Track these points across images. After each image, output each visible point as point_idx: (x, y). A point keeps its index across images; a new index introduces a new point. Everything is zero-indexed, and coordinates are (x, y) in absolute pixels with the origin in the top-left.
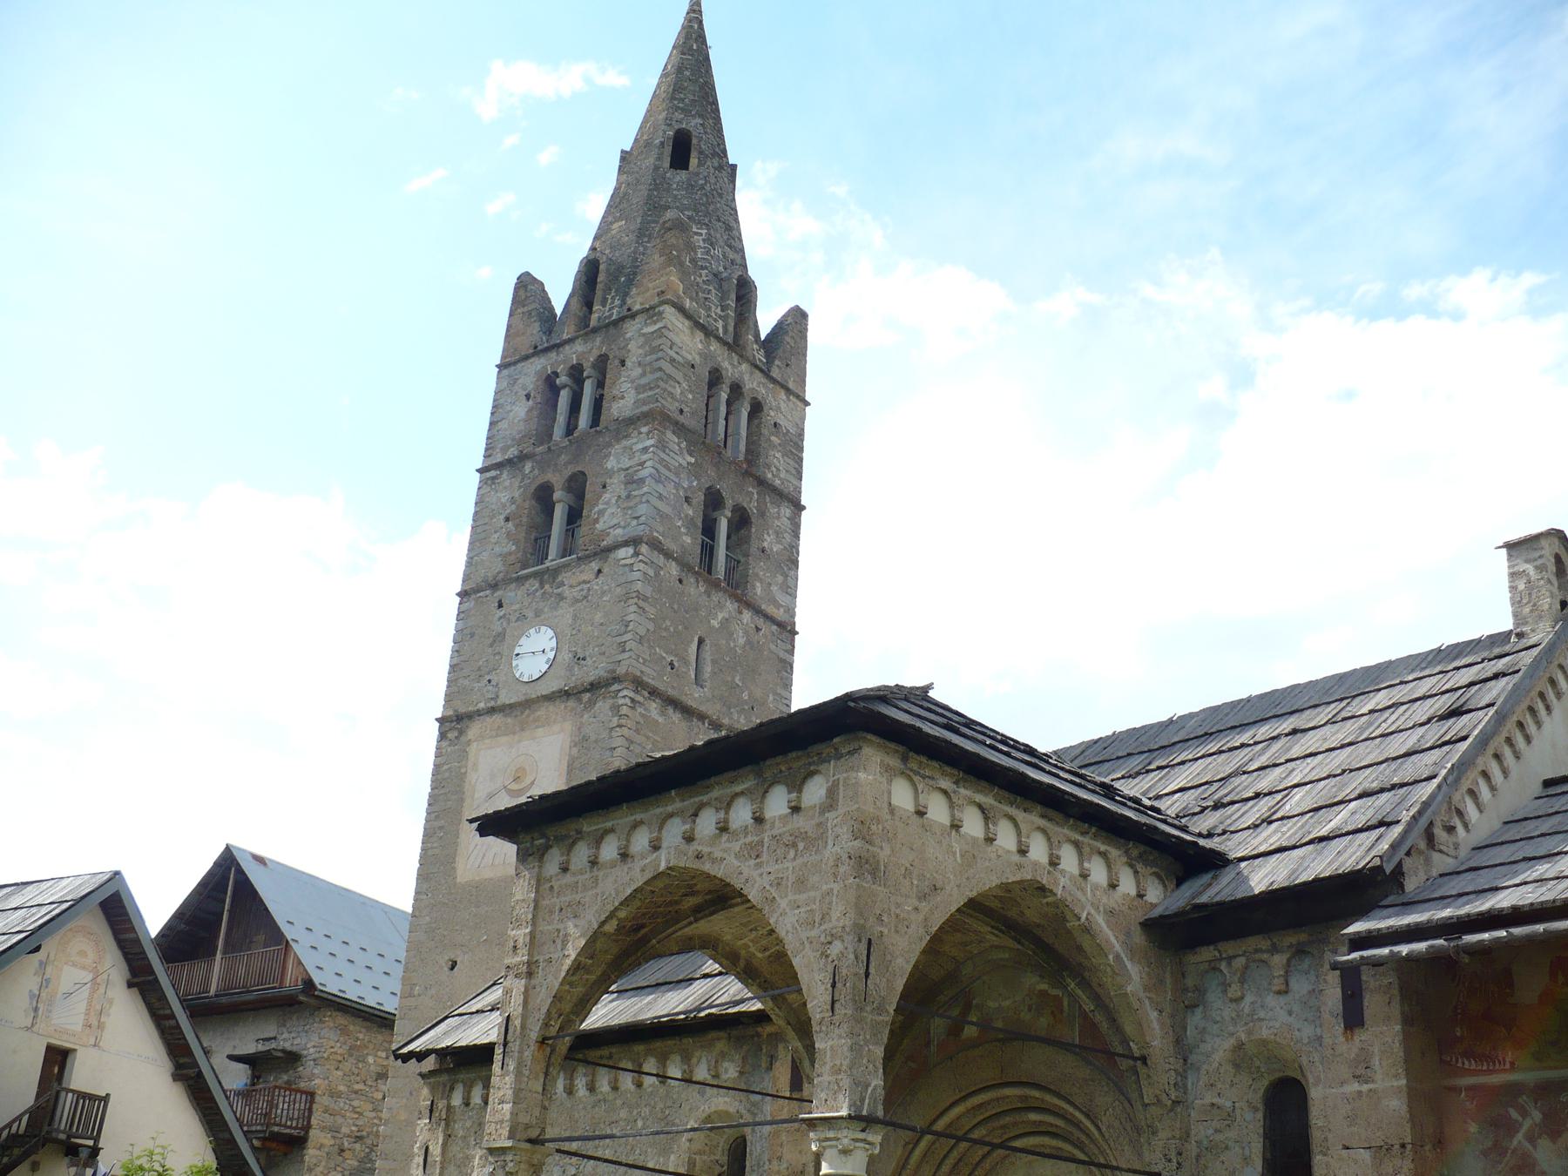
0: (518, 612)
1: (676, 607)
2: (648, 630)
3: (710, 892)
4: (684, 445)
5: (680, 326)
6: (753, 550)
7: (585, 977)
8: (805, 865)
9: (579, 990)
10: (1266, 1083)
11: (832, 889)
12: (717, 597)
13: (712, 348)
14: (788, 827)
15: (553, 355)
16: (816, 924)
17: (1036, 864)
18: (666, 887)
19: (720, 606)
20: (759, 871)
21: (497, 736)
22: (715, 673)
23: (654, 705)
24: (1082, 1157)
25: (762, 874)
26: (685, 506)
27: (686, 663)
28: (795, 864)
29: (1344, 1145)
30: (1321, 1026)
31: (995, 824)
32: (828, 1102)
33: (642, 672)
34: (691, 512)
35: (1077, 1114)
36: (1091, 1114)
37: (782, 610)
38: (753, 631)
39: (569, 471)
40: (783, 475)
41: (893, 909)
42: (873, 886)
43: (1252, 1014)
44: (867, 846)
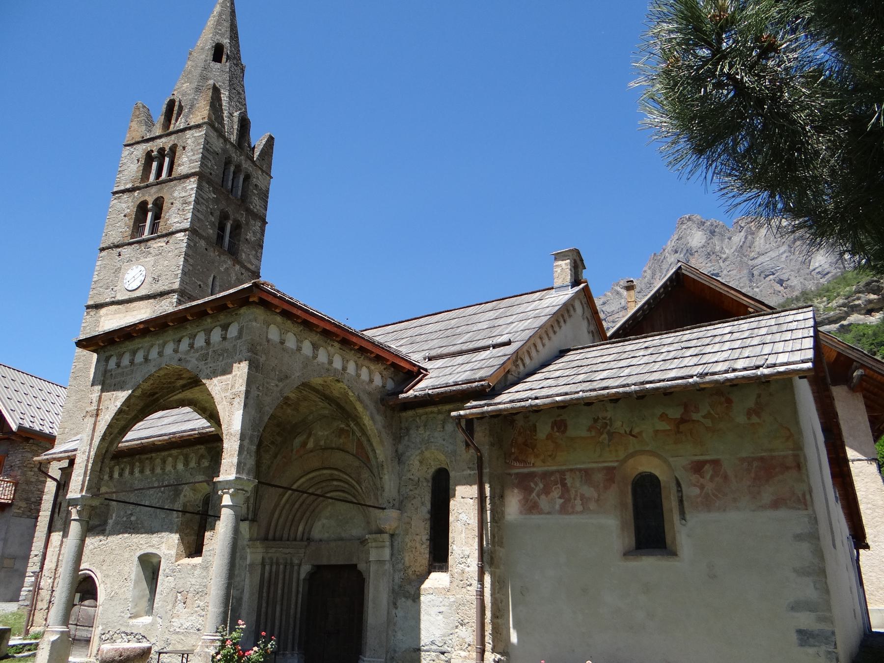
1: (203, 260)
3: (190, 378)
4: (211, 189)
6: (242, 239)
7: (125, 416)
9: (122, 423)
12: (223, 258)
14: (221, 346)
15: (151, 143)
17: (335, 369)
18: (165, 375)
19: (225, 262)
20: (207, 366)
24: (356, 501)
25: (207, 368)
27: (207, 285)
31: (318, 350)
34: (213, 220)
35: (353, 482)
37: (254, 266)
38: (239, 274)
39: (155, 197)
41: (265, 384)
42: (257, 374)
43: (429, 439)
44: (254, 356)
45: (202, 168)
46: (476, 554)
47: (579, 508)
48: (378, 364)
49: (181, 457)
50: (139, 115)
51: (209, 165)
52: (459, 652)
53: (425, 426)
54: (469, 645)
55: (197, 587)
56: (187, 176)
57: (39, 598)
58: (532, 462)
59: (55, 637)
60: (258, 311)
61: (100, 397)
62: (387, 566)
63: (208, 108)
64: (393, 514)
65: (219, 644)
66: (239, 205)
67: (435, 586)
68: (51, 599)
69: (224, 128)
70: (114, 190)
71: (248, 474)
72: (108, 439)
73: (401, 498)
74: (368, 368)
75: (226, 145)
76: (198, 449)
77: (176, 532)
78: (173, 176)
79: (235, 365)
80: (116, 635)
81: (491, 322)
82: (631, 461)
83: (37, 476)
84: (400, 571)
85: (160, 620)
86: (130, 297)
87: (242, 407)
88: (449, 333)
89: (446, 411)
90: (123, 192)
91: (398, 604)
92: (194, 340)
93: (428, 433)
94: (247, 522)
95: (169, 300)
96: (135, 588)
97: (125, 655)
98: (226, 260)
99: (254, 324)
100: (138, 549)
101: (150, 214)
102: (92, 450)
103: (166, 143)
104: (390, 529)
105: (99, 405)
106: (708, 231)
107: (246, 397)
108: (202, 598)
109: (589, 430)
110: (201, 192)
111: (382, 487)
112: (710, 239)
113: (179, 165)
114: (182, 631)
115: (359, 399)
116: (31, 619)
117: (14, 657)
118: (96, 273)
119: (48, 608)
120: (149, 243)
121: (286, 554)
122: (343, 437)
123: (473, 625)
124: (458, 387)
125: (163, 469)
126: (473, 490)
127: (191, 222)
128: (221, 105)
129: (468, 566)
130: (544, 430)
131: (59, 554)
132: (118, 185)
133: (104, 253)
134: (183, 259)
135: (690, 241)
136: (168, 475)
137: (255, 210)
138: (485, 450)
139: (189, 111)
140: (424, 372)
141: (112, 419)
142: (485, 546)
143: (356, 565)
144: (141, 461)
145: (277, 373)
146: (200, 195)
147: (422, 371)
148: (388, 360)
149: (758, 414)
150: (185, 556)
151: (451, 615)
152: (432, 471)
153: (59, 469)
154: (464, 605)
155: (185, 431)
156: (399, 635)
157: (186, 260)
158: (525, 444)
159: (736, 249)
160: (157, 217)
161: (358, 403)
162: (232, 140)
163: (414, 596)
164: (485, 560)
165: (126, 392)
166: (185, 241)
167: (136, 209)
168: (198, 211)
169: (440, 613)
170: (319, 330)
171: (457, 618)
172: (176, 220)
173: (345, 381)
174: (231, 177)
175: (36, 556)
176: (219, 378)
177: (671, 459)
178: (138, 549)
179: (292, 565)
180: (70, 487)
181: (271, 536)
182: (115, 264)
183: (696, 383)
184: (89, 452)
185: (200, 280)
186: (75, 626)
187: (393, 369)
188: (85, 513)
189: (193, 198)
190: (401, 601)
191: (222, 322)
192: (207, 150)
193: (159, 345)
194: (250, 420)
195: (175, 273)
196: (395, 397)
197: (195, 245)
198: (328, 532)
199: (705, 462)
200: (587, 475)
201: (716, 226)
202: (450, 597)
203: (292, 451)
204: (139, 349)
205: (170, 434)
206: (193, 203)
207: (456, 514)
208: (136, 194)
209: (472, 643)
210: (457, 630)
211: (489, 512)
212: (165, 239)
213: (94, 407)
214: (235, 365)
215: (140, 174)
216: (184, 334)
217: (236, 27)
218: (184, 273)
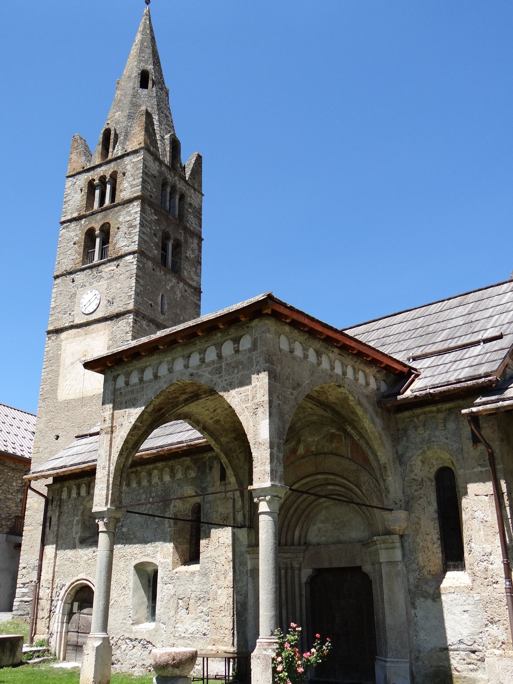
0: (82, 284)
1: (152, 280)
2: (141, 290)
3: (192, 392)
4: (153, 211)
5: (149, 159)
6: (183, 256)
8: (243, 375)
10: (436, 469)
11: (257, 385)
12: (168, 277)
13: (163, 169)
14: (234, 359)
15: (92, 172)
16: (250, 401)
17: (337, 375)
19: (171, 281)
20: (221, 379)
21: (75, 337)
22: (169, 309)
23: (145, 322)
25: (222, 381)
26: (154, 237)
27: (157, 304)
28: (238, 375)
29: (475, 494)
30: (462, 443)
31: (321, 357)
32: (261, 479)
33: (139, 308)
34: (157, 240)
35: (351, 485)
36: (358, 485)
39: (101, 223)
40: (194, 225)
42: (275, 383)
43: (430, 439)
44: (271, 366)
45: (143, 192)
46: (499, 551)
48: (372, 367)
49: (167, 469)
50: (77, 147)
51: (149, 188)
53: (424, 425)
54: (503, 643)
55: (198, 593)
56: (130, 201)
57: (39, 607)
59: (98, 643)
60: (269, 322)
61: (113, 415)
62: (400, 567)
63: (143, 133)
64: (402, 514)
65: (277, 646)
66: (177, 225)
67: (457, 585)
68: (51, 608)
69: (159, 152)
70: (62, 220)
71: (280, 481)
72: (125, 454)
73: (407, 499)
74: (364, 371)
75: (161, 167)
76: (184, 461)
77: (170, 541)
78: (116, 202)
79: (254, 377)
80: (120, 641)
81: (466, 317)
83: (5, 494)
84: (415, 571)
85: (162, 625)
86: (88, 320)
87: (268, 416)
88: (419, 332)
89: (446, 409)
90: (70, 221)
91: (416, 604)
92: (204, 354)
93: (428, 433)
94: (245, 529)
95: (125, 320)
96: (134, 596)
97: (178, 658)
98: (171, 278)
99: (268, 335)
100: (133, 559)
101: (98, 241)
102: (111, 465)
103: (106, 170)
104: (400, 530)
105: (112, 423)
107: (270, 407)
108: (205, 604)
110: (144, 215)
111: (386, 489)
113: (121, 191)
114: (188, 636)
115: (359, 403)
116: (34, 627)
117: (28, 663)
118: (53, 300)
119: (49, 617)
120: (100, 268)
121: (286, 558)
123: (505, 622)
124: (463, 384)
125: (150, 481)
126: (489, 487)
127: (138, 245)
128: (154, 130)
129: (492, 564)
131: (55, 566)
132: (65, 214)
133: (58, 281)
134: (134, 281)
136: (155, 487)
137: (192, 228)
138: (496, 446)
139: (125, 139)
140: (415, 372)
141: (128, 435)
142: (508, 542)
143: (360, 568)
145: (291, 382)
146: (143, 217)
147: (413, 371)
148: (382, 363)
150: (180, 564)
151: (478, 613)
152: (434, 470)
153: (46, 486)
155: (172, 444)
156: (422, 635)
157: (137, 282)
160: (105, 241)
161: (359, 407)
162: (166, 162)
163: (433, 596)
164: (510, 556)
165: (139, 408)
166: (135, 263)
167: (84, 236)
168: (144, 233)
169: (465, 611)
170: (323, 337)
172: (124, 244)
173: (346, 386)
174: (168, 198)
175: (24, 568)
176: (237, 390)
179: (293, 569)
180: (94, 501)
182: (70, 290)
184: (109, 467)
185: (151, 300)
186: (77, 634)
187: (385, 371)
188: (111, 525)
189: (138, 222)
190: (420, 602)
191: (233, 336)
192: (146, 174)
193: (168, 362)
194: (275, 428)
197: (144, 266)
202: (475, 595)
204: (146, 367)
205: (157, 448)
206: (138, 226)
207: (471, 512)
208: (83, 222)
209: (506, 641)
210: (487, 629)
211: (508, 509)
212: (115, 263)
213: (108, 424)
214: (254, 377)
215: (84, 202)
216: (194, 350)
217: (157, 52)
218: (137, 294)
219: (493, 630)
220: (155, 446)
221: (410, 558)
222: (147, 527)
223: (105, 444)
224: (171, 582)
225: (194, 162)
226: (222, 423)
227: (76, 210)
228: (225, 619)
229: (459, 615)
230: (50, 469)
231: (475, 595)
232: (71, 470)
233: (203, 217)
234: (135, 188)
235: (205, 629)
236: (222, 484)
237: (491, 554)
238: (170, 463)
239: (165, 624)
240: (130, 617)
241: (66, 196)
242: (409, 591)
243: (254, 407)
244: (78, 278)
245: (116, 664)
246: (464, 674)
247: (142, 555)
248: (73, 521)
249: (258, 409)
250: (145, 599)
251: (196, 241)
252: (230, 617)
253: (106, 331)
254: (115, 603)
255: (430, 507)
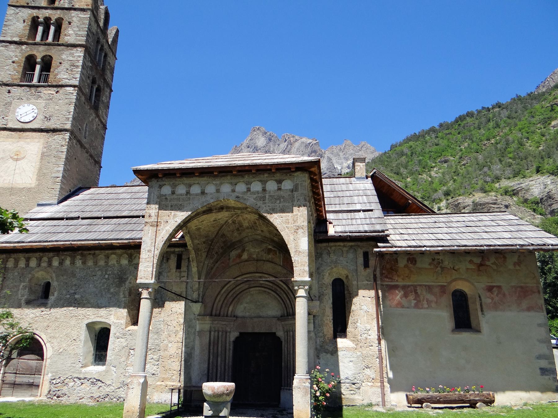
10: (333, 279)
14: (277, 194)
20: (265, 205)
23: (75, 141)
27: (83, 129)
28: (280, 205)
43: (336, 261)
46: (376, 328)
47: (426, 306)
51: (90, 41)
52: (367, 383)
58: (396, 279)
77: (124, 308)
79: (295, 209)
82: (454, 283)
86: (23, 127)
89: (349, 246)
90: (11, 42)
96: (84, 346)
101: (38, 67)
106: (268, 138)
109: (430, 264)
112: (268, 143)
121: (223, 325)
122: (271, 254)
126: (372, 293)
129: (369, 336)
130: (402, 263)
134: (73, 108)
135: (257, 142)
143: (275, 333)
144: (82, 255)
149: (519, 265)
150: (131, 324)
151: (358, 363)
154: (368, 357)
158: (391, 269)
159: (281, 152)
165: (185, 213)
166: (75, 94)
171: (364, 364)
172: (65, 77)
177: (476, 284)
178: (86, 319)
181: (214, 313)
182: (5, 99)
183: (518, 249)
191: (277, 178)
195: (66, 116)
196: (325, 234)
198: (249, 312)
199: (493, 287)
200: (429, 288)
201: (272, 136)
202: (357, 352)
203: (229, 259)
206: (81, 67)
210: (364, 371)
212: (55, 89)
214: (295, 209)
215: (27, 32)
219: (367, 371)
220: (125, 238)
221: (318, 329)
222: (102, 296)
223: (150, 233)
224: (123, 337)
225: (114, 33)
226: (201, 230)
227: (17, 35)
228: (173, 364)
229: (347, 363)
230: (4, 242)
231: (357, 352)
232: (31, 246)
233: (114, 75)
234: (80, 38)
235: (154, 370)
236: (177, 271)
237: (369, 330)
238: (129, 251)
239: (115, 367)
240: (79, 362)
241: (7, 20)
242: (316, 349)
243: (295, 228)
244: (14, 91)
245: (62, 397)
246: (347, 396)
247: (95, 316)
248: (19, 286)
249: (299, 230)
250: (92, 349)
251: (109, 91)
252: (178, 362)
253: (41, 140)
254: (64, 351)
255: (330, 300)
